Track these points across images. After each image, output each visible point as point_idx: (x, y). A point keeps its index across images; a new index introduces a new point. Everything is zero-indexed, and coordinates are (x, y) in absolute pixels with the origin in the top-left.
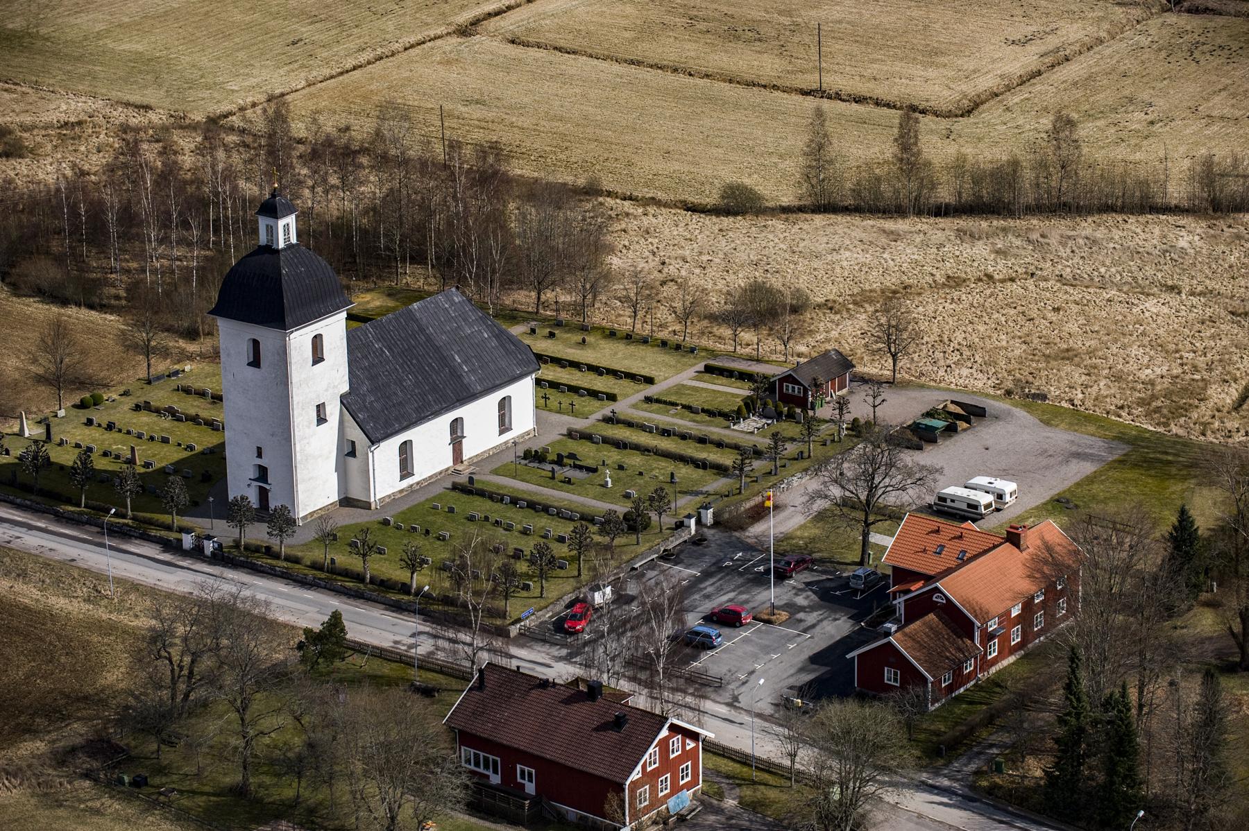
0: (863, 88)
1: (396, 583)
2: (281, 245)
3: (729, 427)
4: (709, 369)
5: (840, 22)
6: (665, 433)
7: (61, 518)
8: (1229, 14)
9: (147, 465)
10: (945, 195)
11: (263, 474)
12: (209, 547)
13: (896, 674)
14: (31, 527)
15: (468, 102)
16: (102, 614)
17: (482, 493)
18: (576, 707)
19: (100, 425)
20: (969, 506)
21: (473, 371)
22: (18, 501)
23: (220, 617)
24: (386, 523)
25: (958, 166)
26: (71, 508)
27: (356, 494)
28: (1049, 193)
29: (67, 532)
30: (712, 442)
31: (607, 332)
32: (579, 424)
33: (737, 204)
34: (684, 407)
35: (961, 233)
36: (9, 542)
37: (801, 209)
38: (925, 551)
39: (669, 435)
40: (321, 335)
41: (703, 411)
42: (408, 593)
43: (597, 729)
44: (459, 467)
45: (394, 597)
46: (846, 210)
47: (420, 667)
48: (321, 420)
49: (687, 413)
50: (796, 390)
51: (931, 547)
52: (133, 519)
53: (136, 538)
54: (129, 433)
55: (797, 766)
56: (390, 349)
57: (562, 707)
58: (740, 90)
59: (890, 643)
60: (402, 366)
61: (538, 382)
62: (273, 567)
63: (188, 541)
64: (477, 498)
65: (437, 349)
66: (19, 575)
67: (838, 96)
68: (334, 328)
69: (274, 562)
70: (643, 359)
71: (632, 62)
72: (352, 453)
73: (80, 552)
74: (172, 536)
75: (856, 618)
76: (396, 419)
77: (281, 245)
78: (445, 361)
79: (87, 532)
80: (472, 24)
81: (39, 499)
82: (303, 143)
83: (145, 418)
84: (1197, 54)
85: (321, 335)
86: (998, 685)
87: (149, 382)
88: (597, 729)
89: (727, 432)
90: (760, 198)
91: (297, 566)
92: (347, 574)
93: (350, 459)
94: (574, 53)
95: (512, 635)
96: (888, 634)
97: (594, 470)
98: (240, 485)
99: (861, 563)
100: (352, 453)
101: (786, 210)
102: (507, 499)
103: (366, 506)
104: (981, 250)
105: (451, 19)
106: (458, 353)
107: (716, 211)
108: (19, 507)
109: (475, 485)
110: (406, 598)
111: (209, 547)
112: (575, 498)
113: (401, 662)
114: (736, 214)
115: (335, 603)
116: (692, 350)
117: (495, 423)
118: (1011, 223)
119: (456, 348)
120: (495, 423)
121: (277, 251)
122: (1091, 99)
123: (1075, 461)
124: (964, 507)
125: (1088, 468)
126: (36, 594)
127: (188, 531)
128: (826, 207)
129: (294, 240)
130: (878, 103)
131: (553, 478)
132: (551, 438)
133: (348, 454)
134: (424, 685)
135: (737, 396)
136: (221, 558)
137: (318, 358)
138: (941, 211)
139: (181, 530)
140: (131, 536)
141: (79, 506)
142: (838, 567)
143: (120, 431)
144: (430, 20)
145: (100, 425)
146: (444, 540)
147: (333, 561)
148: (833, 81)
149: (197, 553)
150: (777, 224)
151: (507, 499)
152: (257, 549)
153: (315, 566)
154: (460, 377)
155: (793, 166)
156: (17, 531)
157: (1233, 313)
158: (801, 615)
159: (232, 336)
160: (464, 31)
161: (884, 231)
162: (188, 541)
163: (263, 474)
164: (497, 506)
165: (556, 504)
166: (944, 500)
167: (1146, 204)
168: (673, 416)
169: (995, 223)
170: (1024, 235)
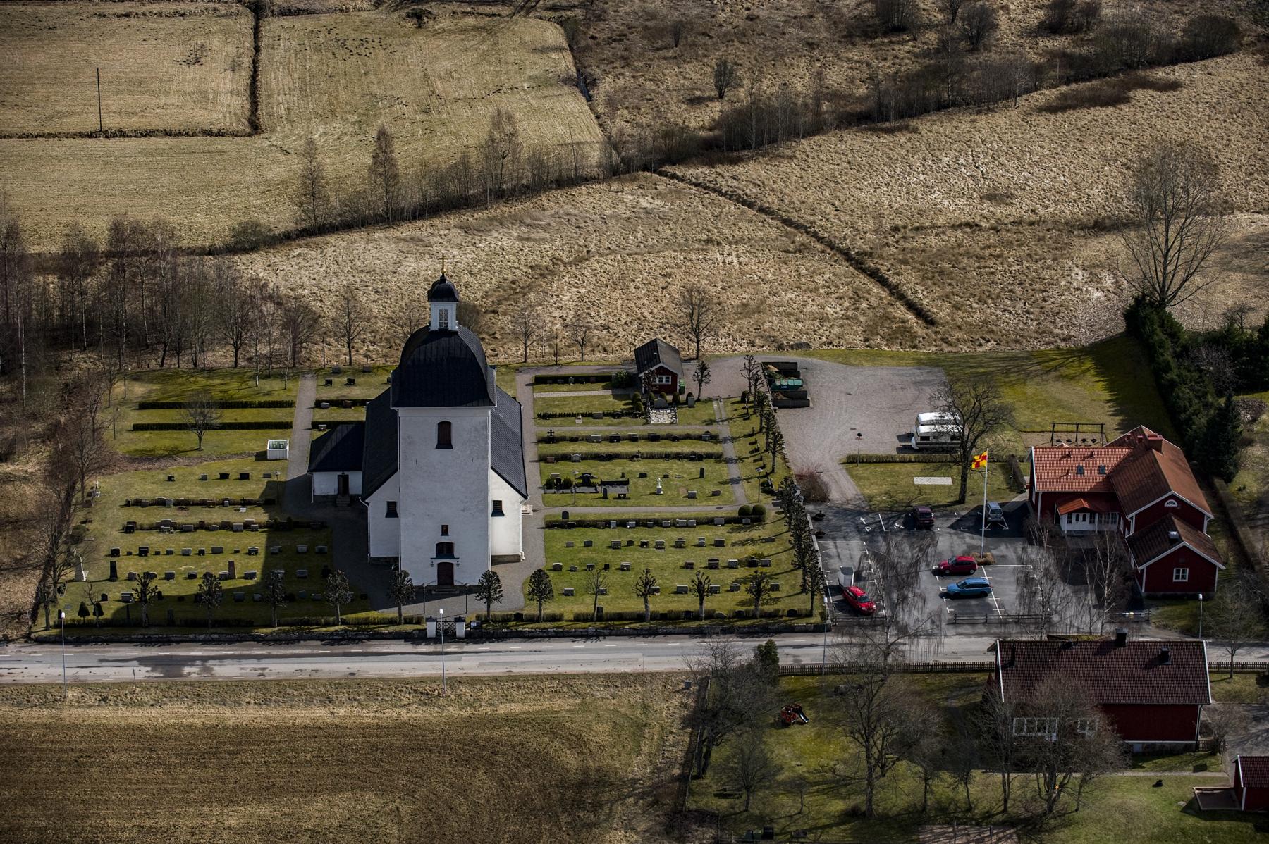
4: (539, 381)
6: (613, 439)
11: (445, 550)
12: (461, 629)
18: (1112, 655)
19: (129, 553)
22: (202, 637)
26: (269, 630)
29: (296, 652)
34: (584, 415)
36: (262, 675)
40: (449, 424)
41: (604, 415)
53: (368, 639)
54: (201, 553)
57: (1099, 659)
58: (172, 141)
59: (1184, 547)
63: (431, 628)
67: (122, 134)
69: (537, 625)
74: (409, 628)
79: (306, 647)
85: (449, 424)
91: (564, 623)
92: (620, 617)
94: (55, 136)
102: (613, 523)
109: (571, 518)
111: (461, 629)
121: (456, 333)
131: (605, 497)
140: (361, 640)
143: (158, 553)
145: (129, 553)
147: (600, 610)
148: (112, 123)
149: (447, 635)
151: (613, 523)
152: (506, 619)
153: (578, 618)
162: (431, 628)
163: (445, 550)
167: (568, 181)
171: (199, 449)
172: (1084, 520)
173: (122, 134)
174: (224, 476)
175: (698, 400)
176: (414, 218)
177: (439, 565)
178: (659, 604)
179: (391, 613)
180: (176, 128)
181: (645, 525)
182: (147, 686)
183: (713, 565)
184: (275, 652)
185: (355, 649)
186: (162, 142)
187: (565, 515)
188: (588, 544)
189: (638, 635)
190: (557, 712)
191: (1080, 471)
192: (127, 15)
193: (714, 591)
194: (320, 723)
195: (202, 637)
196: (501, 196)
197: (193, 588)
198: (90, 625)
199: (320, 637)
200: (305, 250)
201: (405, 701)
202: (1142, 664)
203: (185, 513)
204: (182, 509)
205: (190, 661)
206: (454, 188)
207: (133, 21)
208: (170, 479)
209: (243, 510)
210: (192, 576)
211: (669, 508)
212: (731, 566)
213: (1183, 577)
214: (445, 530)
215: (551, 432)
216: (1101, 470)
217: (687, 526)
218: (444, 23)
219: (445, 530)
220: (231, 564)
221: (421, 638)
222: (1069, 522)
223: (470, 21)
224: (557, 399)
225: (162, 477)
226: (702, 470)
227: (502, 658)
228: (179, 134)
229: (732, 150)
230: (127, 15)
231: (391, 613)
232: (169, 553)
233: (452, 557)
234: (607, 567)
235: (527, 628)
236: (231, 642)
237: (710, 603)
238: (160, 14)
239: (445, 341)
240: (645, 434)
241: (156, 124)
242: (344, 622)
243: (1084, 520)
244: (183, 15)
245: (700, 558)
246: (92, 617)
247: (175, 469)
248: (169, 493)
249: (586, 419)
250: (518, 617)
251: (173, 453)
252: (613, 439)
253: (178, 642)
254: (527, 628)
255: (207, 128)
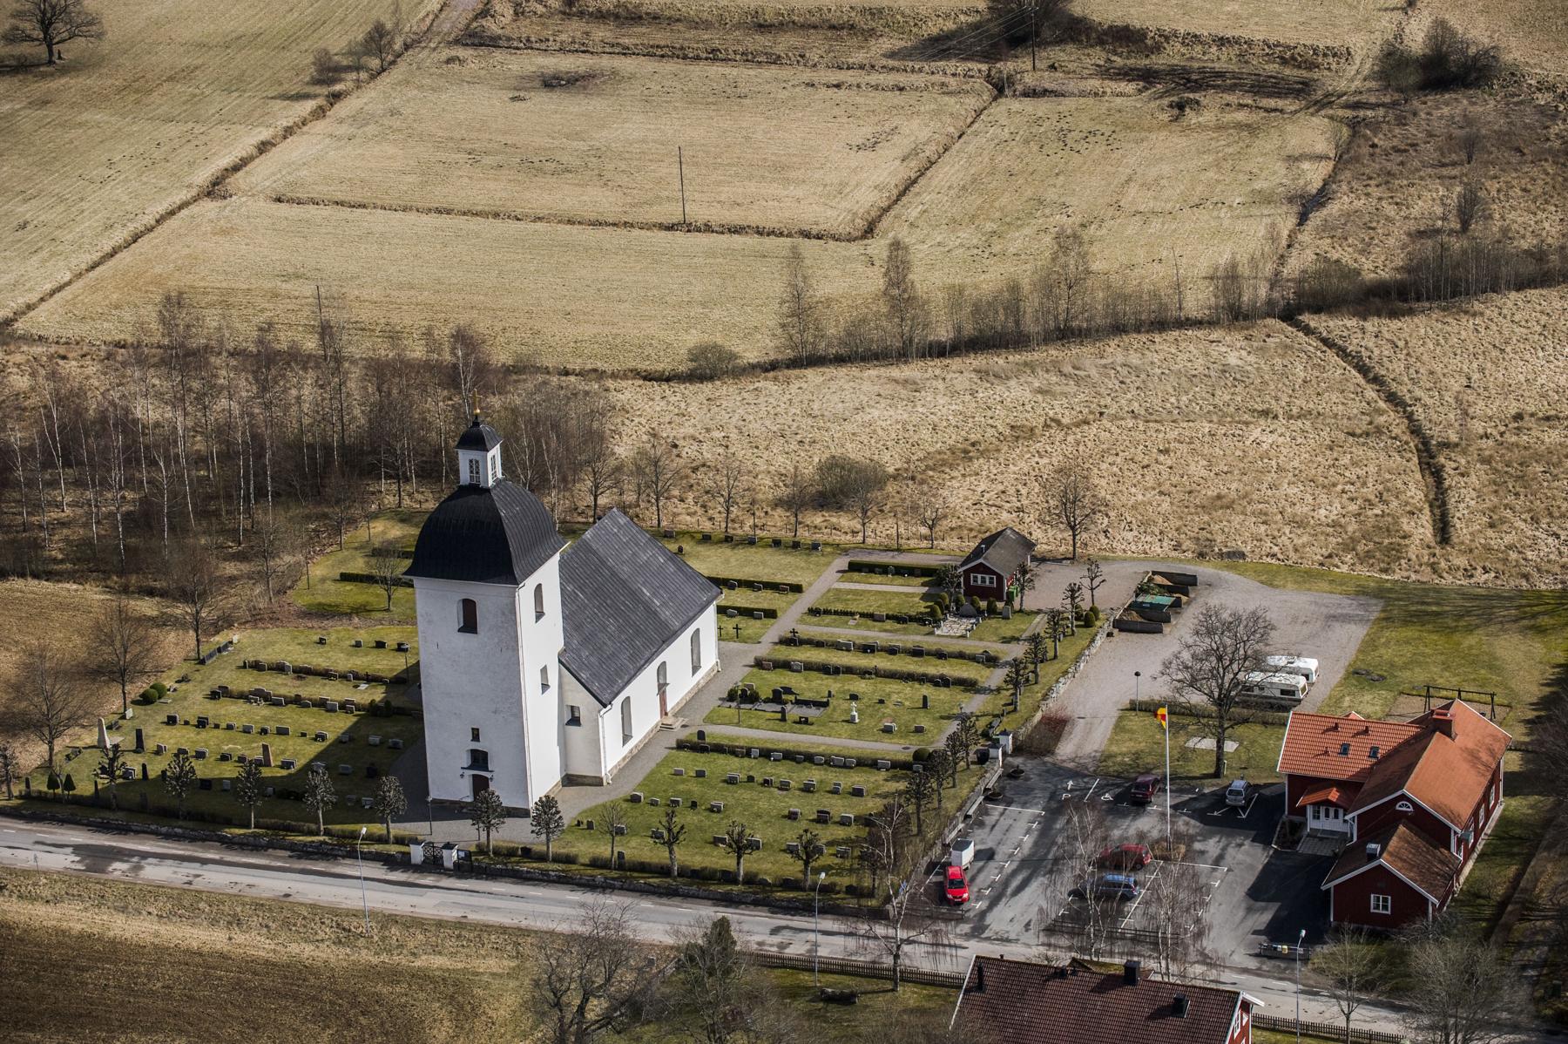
0: (735, 217)
1: (715, 871)
2: (491, 483)
3: (932, 633)
4: (854, 567)
5: (644, 141)
6: (867, 649)
7: (230, 844)
8: (1072, 94)
9: (286, 765)
10: (943, 334)
11: (479, 759)
13: (1385, 900)
14: (204, 862)
15: (286, 277)
16: (367, 957)
17: (719, 749)
18: (1113, 994)
20: (1283, 692)
21: (664, 604)
22: (164, 830)
23: (604, 948)
24: (635, 799)
25: (956, 295)
26: (242, 831)
27: (581, 768)
28: (1056, 318)
29: (245, 860)
30: (929, 653)
31: (700, 536)
32: (763, 650)
33: (708, 368)
34: (863, 615)
35: (983, 374)
36: (190, 883)
37: (773, 366)
38: (1326, 753)
39: (873, 651)
41: (888, 617)
42: (735, 881)
43: (1152, 1017)
44: (669, 721)
45: (722, 889)
46: (840, 360)
47: (822, 971)
48: (545, 687)
49: (870, 622)
50: (987, 581)
51: (1334, 748)
52: (327, 833)
53: (344, 857)
55: (1352, 1026)
56: (583, 592)
57: (1095, 997)
59: (1380, 867)
60: (599, 608)
61: (722, 610)
62: (545, 873)
63: (417, 854)
64: (715, 755)
65: (624, 583)
66: (230, 923)
67: (708, 228)
68: (548, 575)
69: (542, 865)
70: (764, 563)
71: (439, 211)
72: (575, 721)
73: (291, 884)
74: (393, 849)
75: (1263, 839)
76: (617, 674)
77: (491, 483)
78: (635, 596)
80: (214, 184)
81: (191, 824)
82: (123, 347)
83: (232, 711)
84: (1070, 142)
86: (1478, 896)
87: (202, 662)
88: (1152, 1017)
89: (930, 639)
90: (733, 356)
91: (574, 867)
92: (643, 868)
93: (572, 728)
95: (891, 914)
96: (1372, 857)
97: (826, 705)
98: (448, 779)
99: (1217, 774)
100: (575, 721)
101: (773, 366)
102: (755, 752)
103: (597, 782)
104: (1017, 391)
105: (187, 180)
106: (644, 584)
107: (693, 377)
108: (168, 837)
110: (735, 888)
112: (815, 739)
113: (785, 967)
114: (711, 378)
115: (710, 913)
116: (815, 547)
117: (692, 665)
118: (1026, 356)
119: (641, 580)
120: (692, 665)
121: (488, 490)
122: (997, 204)
123: (1337, 625)
124: (1278, 695)
125: (1358, 632)
126: (269, 945)
127: (416, 842)
128: (815, 361)
129: (500, 476)
130: (760, 232)
131: (783, 719)
132: (738, 676)
133: (570, 723)
134: (838, 992)
135: (913, 595)
136: (470, 868)
137: (540, 615)
138: (939, 351)
139: (400, 841)
140: (335, 857)
141: (248, 827)
142: (1194, 783)
143: (217, 726)
144: (163, 183)
145: (187, 723)
146: (719, 811)
147: (621, 855)
148: (698, 213)
149: (433, 865)
150: (766, 384)
151: (755, 752)
152: (511, 853)
153: (596, 863)
154: (655, 613)
155: (770, 317)
156: (193, 868)
157: (1353, 435)
158: (1197, 846)
159: (436, 603)
160: (215, 189)
161: (896, 381)
162: (417, 854)
163: (479, 759)
164: (746, 761)
165: (821, 750)
166: (1250, 689)
168: (827, 626)
169: (1011, 358)
170: (1056, 368)
171: (388, 610)
172: (1327, 816)
173: (708, 228)
174: (380, 645)
175: (1021, 611)
176: (924, 356)
177: (474, 776)
178: (688, 856)
179: (378, 829)
180: (769, 225)
181: (794, 759)
182: (64, 875)
183: (823, 818)
184: (228, 858)
185: (320, 866)
186: (751, 241)
187: (701, 735)
188: (700, 774)
189: (654, 893)
190: (477, 974)
191: (1345, 750)
192: (838, 86)
193: (754, 846)
194: (205, 949)
195: (164, 830)
196: (1065, 334)
197: (230, 771)
198: (57, 800)
199: (292, 847)
200: (769, 384)
201: (321, 935)
202: (1147, 1011)
203: (298, 683)
204: (299, 678)
205: (121, 855)
206: (1000, 320)
207: (842, 93)
208: (322, 642)
209: (363, 686)
210: (224, 758)
211: (854, 743)
212: (844, 822)
213: (1385, 907)
214: (476, 735)
215: (794, 632)
216: (1374, 752)
217: (845, 766)
218: (1208, 117)
219: (476, 735)
220: (265, 748)
221: (403, 863)
222: (1316, 817)
223: (1241, 116)
224: (855, 592)
225: (316, 638)
226: (925, 698)
227: (521, 905)
228: (771, 233)
229: (1406, 301)
230: (838, 86)
231: (378, 829)
232: (230, 727)
233: (486, 769)
234: (694, 805)
235: (525, 867)
236: (193, 840)
237: (749, 863)
238: (876, 87)
239: (472, 499)
240: (910, 645)
241: (754, 218)
242: (327, 832)
243: (1327, 816)
244: (901, 89)
245: (808, 807)
246: (59, 791)
247: (338, 632)
248: (318, 660)
249: (863, 620)
250: (527, 853)
251: (362, 610)
252: (867, 649)
253: (137, 832)
254: (525, 867)
255: (807, 228)
